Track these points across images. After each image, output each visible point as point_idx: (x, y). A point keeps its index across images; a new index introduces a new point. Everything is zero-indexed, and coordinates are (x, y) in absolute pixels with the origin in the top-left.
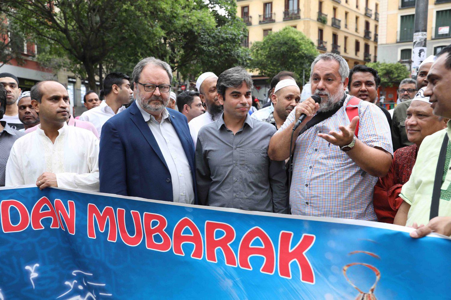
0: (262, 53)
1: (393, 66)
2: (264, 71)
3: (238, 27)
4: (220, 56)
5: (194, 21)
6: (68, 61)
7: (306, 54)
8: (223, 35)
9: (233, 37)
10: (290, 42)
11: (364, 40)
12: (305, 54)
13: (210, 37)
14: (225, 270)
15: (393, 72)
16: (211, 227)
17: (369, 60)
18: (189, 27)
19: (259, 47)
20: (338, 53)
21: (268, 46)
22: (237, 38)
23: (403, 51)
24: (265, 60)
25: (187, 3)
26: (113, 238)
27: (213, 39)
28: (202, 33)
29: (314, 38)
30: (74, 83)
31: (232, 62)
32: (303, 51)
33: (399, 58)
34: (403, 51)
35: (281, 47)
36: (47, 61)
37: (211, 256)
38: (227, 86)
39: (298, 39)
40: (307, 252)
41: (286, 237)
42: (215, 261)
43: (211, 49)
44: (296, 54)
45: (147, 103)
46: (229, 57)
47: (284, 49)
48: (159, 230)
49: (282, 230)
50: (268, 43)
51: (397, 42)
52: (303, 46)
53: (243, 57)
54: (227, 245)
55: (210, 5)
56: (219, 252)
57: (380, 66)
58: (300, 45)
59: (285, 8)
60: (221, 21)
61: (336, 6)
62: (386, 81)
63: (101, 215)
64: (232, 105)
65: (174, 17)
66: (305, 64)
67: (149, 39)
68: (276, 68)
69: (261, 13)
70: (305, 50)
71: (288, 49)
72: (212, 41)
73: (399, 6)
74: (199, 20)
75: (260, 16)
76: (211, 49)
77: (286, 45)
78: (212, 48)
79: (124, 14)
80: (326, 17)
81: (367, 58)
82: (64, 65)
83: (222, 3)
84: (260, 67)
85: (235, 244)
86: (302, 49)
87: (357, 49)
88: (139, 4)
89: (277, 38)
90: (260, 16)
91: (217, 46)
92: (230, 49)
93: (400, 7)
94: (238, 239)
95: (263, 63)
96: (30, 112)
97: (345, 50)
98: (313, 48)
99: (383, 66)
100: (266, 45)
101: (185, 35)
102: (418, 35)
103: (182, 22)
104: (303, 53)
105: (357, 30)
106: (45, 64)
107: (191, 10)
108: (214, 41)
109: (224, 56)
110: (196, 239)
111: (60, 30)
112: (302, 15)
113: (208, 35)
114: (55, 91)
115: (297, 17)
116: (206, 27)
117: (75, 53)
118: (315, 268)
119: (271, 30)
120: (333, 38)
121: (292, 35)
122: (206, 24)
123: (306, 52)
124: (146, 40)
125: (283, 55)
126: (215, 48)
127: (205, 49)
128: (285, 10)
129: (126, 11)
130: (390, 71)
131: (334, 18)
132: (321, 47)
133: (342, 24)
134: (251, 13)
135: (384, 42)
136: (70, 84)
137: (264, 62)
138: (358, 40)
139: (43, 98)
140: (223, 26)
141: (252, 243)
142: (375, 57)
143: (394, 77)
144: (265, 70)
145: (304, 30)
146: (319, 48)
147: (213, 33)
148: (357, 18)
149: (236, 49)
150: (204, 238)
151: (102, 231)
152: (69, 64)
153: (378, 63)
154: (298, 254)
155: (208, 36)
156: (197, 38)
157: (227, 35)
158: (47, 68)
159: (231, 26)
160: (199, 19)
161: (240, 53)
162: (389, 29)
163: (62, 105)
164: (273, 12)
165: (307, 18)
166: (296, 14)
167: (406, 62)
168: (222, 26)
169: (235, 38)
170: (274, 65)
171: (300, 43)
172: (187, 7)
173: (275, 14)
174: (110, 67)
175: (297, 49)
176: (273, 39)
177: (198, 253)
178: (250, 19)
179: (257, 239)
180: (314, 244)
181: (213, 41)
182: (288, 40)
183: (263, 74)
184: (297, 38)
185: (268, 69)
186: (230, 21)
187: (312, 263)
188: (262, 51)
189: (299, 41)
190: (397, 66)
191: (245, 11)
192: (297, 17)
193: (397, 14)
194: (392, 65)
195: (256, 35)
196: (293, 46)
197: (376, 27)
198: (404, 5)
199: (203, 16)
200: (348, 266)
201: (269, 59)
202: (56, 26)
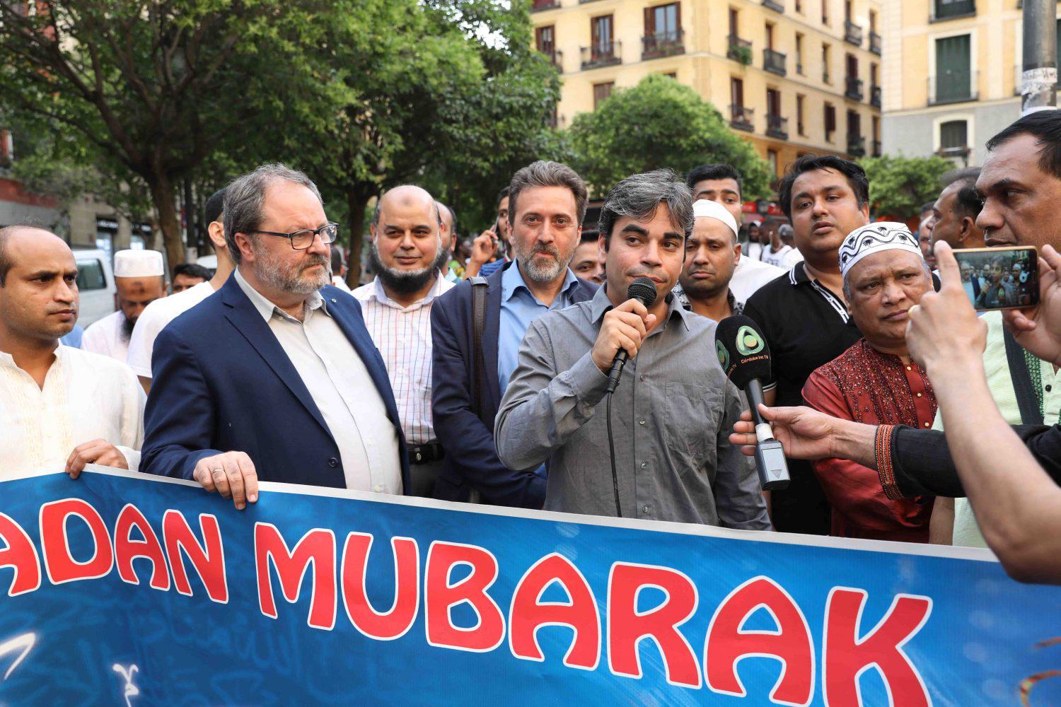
0: (597, 142)
1: (923, 166)
2: (603, 187)
3: (538, 77)
4: (497, 150)
5: (430, 64)
6: (97, 176)
7: (710, 140)
8: (502, 98)
9: (525, 103)
10: (666, 113)
11: (846, 101)
12: (706, 141)
14: (663, 698)
15: (923, 179)
16: (627, 580)
17: (861, 153)
18: (414, 78)
19: (583, 126)
20: (784, 136)
21: (612, 123)
22: (538, 104)
23: (944, 126)
24: (606, 160)
25: (409, 19)
26: (323, 617)
27: (475, 109)
28: (449, 96)
29: (721, 101)
30: (113, 232)
32: (701, 133)
33: (936, 144)
34: (944, 126)
35: (645, 125)
36: (42, 176)
37: (624, 660)
38: (617, 211)
39: (687, 103)
40: (910, 642)
41: (845, 606)
42: (637, 673)
44: (683, 143)
45: (296, 276)
47: (652, 129)
48: (472, 590)
49: (836, 585)
50: (611, 116)
51: (930, 105)
52: (700, 120)
53: (554, 153)
54: (672, 629)
55: (465, 24)
56: (649, 649)
57: (889, 166)
59: (646, 28)
60: (494, 62)
61: (773, 17)
62: (906, 202)
63: (291, 555)
65: (376, 54)
67: (319, 112)
69: (587, 42)
70: (705, 131)
72: (473, 113)
73: (930, 17)
74: (441, 62)
75: (583, 50)
79: (253, 48)
80: (748, 47)
81: (855, 148)
82: (88, 187)
83: (495, 17)
85: (695, 628)
86: (697, 130)
87: (830, 125)
88: (290, 22)
89: (634, 103)
90: (583, 50)
91: (488, 127)
92: (521, 134)
93: (933, 18)
94: (706, 610)
95: (601, 166)
97: (800, 130)
98: (723, 127)
99: (899, 165)
100: (608, 122)
101: (402, 99)
102: (1034, 77)
103: (398, 68)
104: (701, 138)
105: (826, 77)
106: (37, 186)
107: (421, 37)
110: (582, 615)
111: (83, 94)
112: (688, 42)
113: (463, 98)
114: (44, 258)
115: (676, 48)
116: (458, 77)
117: (122, 152)
118: (933, 688)
119: (611, 83)
120: (768, 100)
121: (673, 94)
122: (459, 71)
123: (707, 135)
124: (307, 116)
126: (482, 130)
128: (646, 34)
129: (255, 39)
130: (916, 177)
131: (770, 53)
133: (790, 65)
134: (559, 45)
135: (898, 106)
136: (101, 234)
137: (603, 164)
138: (831, 103)
139: (11, 275)
140: (500, 75)
141: (747, 623)
142: (876, 144)
143: (926, 191)
144: (606, 184)
145: (695, 81)
146: (735, 124)
147: (476, 93)
148: (826, 47)
149: (535, 132)
150: (605, 611)
151: (293, 599)
152: (99, 183)
153: (886, 158)
154: (882, 648)
155: (463, 102)
156: (435, 108)
157: (513, 99)
158: (42, 194)
159: (520, 76)
160: (441, 58)
161: (547, 144)
162: (906, 77)
163: (60, 297)
164: (617, 37)
165: (702, 51)
166: (673, 43)
167: (954, 154)
168: (497, 75)
169: (531, 106)
171: (693, 112)
172: (409, 28)
173: (620, 43)
174: (205, 189)
176: (625, 105)
177: (585, 653)
178: (558, 58)
179: (762, 610)
180: (929, 621)
181: (477, 115)
182: (662, 107)
183: (602, 195)
184: (684, 100)
186: (516, 62)
187: (928, 676)
188: (597, 136)
189: (690, 109)
190: (934, 165)
191: (545, 38)
192: (676, 48)
193: (927, 35)
194: (921, 162)
195: (575, 101)
196: (676, 122)
197: (874, 68)
198: (942, 13)
199: (452, 50)
200: (1035, 678)
201: (617, 157)
202: (73, 86)
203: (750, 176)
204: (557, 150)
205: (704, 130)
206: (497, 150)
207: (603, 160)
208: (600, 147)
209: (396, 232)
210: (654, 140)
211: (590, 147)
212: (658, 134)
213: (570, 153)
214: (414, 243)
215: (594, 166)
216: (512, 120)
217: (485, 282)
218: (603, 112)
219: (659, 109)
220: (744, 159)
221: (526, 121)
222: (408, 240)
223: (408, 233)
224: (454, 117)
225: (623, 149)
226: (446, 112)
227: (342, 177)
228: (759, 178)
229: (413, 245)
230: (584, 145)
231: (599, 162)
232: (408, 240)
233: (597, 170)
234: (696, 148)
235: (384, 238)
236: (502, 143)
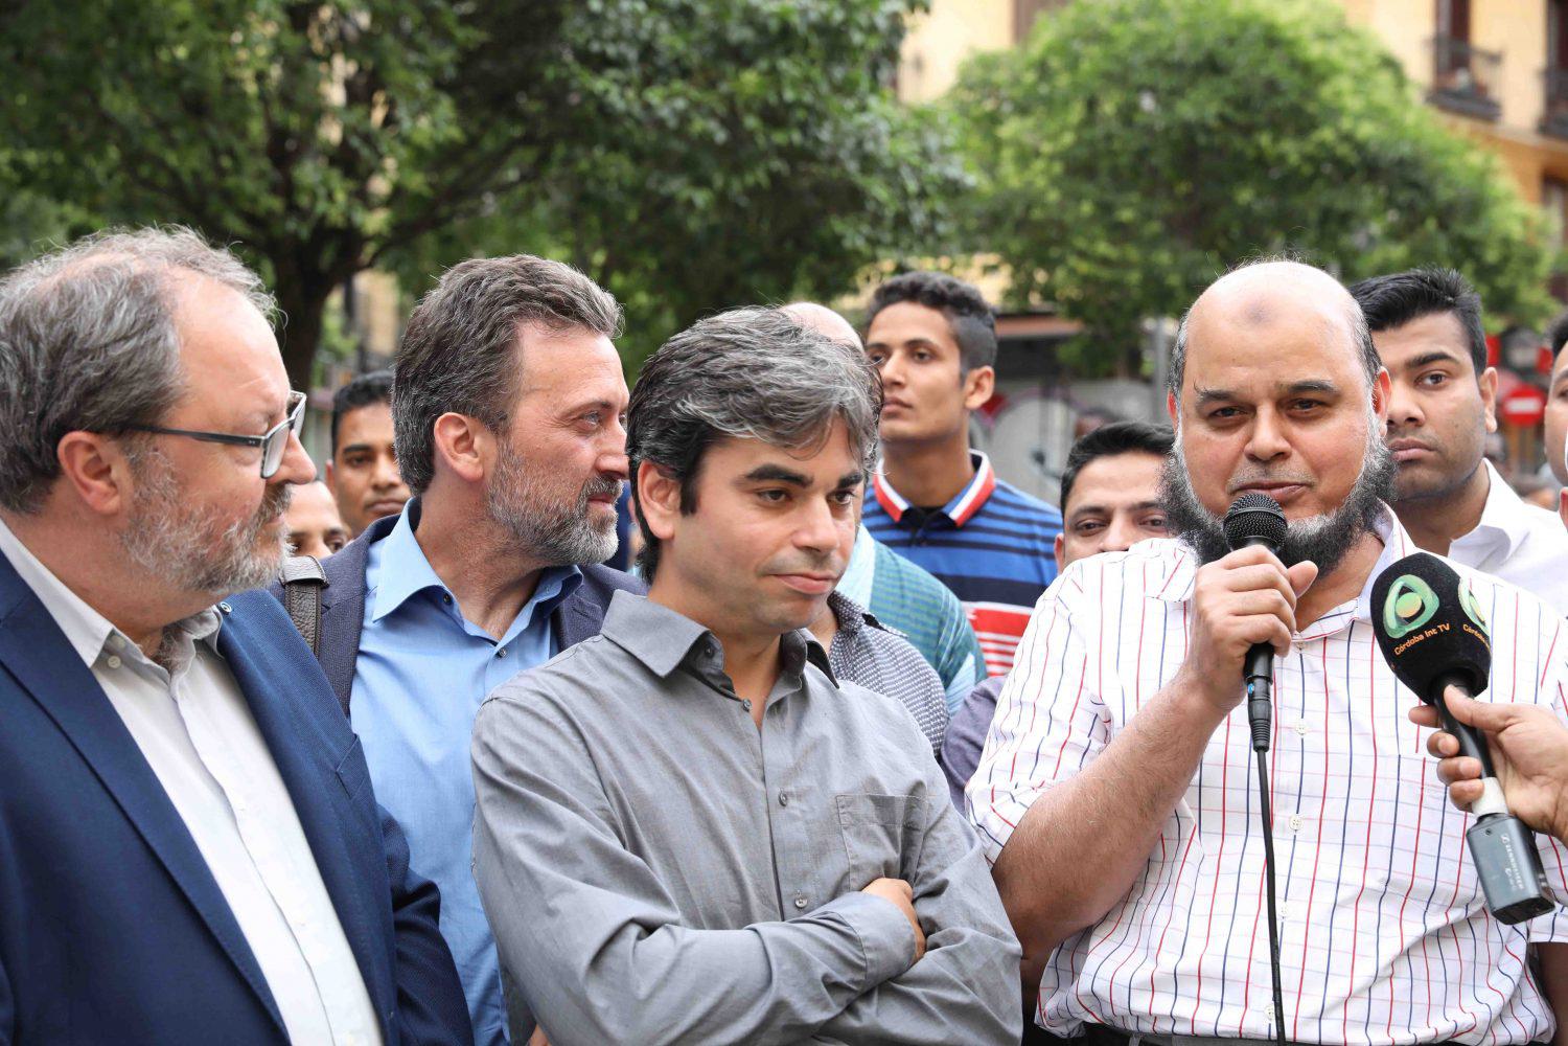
0: (1029, 140)
2: (1041, 276)
4: (736, 153)
7: (1373, 148)
9: (826, 18)
10: (1241, 61)
12: (1360, 147)
13: (655, 14)
21: (1076, 86)
24: (1053, 196)
27: (675, 28)
31: (816, 203)
32: (1346, 124)
35: (1176, 93)
39: (1306, 31)
43: (667, 101)
46: (802, 167)
47: (1200, 106)
52: (1343, 83)
53: (905, 172)
58: (1322, 79)
64: (740, 555)
66: (1364, 221)
68: (1133, 253)
70: (1359, 117)
71: (1229, 111)
72: (670, 41)
76: (667, 101)
77: (1216, 81)
78: (669, 97)
84: (1016, 246)
86: (1333, 113)
89: (1145, 26)
91: (711, 84)
92: (809, 109)
95: (1037, 214)
96: (1417, 413)
98: (1406, 103)
100: (1063, 81)
104: (1347, 138)
108: (688, 42)
109: (763, 156)
123: (1366, 130)
125: (1190, 151)
126: (694, 93)
127: (616, 100)
132: (1458, 95)
137: (1044, 206)
144: (1050, 265)
146: (1444, 97)
161: (885, 140)
170: (1121, 233)
171: (1325, 61)
175: (1296, 111)
176: (1117, 30)
182: (1231, 41)
185: (1073, 261)
188: (1030, 122)
189: (1314, 51)
196: (1272, 87)
201: (1088, 188)
203: (1492, 256)
204: (915, 160)
205: (1357, 113)
206: (736, 153)
207: (1043, 193)
208: (1037, 154)
209: (1229, 411)
210: (1202, 139)
211: (1007, 154)
212: (1213, 122)
213: (953, 172)
214: (1288, 439)
215: (1018, 210)
216: (784, 64)
217: (318, 575)
218: (1050, 50)
219: (1224, 49)
220: (1475, 206)
221: (826, 72)
222: (1266, 433)
223: (1266, 411)
224: (611, 50)
225: (1104, 165)
226: (589, 31)
227: (270, 213)
228: (1513, 266)
229: (1283, 445)
230: (987, 147)
231: (1032, 201)
232: (1266, 433)
233: (1022, 225)
234: (1328, 168)
235: (1201, 430)
236: (751, 134)
